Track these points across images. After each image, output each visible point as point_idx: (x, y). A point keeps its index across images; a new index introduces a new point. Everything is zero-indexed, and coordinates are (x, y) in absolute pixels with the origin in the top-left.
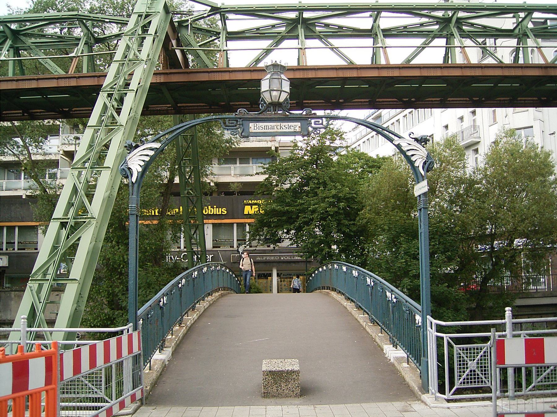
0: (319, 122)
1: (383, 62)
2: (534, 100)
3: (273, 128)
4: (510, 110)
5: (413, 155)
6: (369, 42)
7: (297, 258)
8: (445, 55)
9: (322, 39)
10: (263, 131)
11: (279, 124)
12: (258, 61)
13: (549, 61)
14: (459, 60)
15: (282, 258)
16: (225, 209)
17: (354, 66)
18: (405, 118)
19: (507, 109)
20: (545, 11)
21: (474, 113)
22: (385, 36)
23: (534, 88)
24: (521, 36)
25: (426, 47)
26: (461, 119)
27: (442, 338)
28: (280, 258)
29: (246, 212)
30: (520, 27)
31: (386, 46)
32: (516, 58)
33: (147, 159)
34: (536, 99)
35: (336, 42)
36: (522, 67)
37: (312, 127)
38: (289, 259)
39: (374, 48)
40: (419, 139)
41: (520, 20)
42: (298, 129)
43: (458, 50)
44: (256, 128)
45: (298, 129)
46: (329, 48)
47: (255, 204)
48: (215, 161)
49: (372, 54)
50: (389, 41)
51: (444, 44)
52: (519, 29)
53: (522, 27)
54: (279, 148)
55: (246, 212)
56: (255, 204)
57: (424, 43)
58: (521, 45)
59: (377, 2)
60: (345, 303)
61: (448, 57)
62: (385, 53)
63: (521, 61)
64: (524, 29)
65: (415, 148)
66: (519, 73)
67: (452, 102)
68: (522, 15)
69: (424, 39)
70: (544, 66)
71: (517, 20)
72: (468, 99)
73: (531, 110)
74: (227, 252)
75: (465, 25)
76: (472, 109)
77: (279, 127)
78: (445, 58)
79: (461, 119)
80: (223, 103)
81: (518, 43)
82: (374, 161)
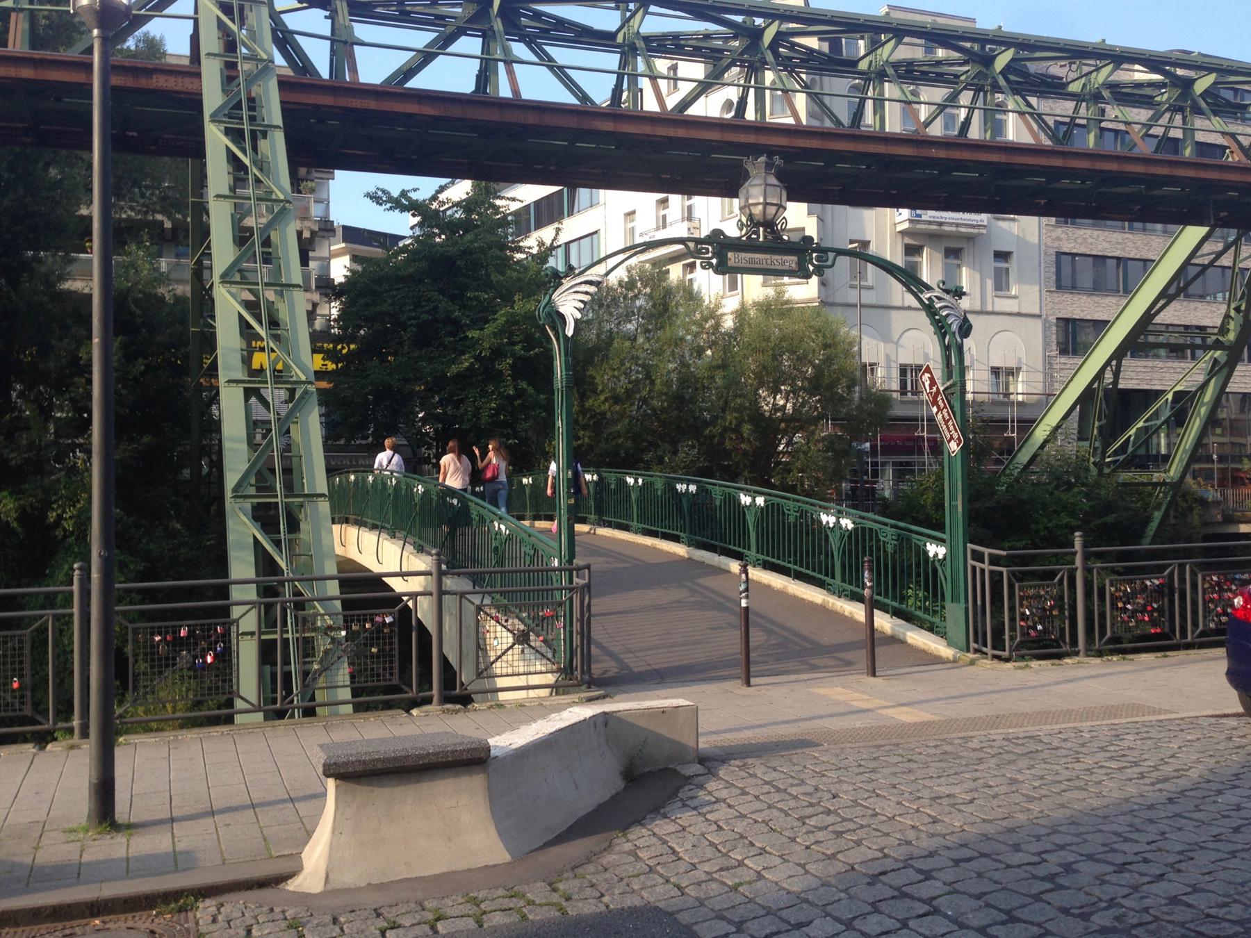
1: (505, 91)
3: (760, 262)
6: (611, 60)
8: (616, 86)
10: (748, 265)
11: (768, 256)
12: (409, 72)
19: (710, 198)
21: (664, 202)
25: (439, 54)
26: (631, 214)
27: (1001, 573)
32: (858, 114)
33: (586, 298)
35: (562, 55)
41: (628, 14)
43: (501, 65)
46: (547, 66)
51: (615, 67)
52: (871, 61)
59: (1104, 41)
62: (511, 73)
63: (750, 115)
71: (623, 15)
72: (650, 175)
75: (784, 47)
76: (661, 196)
77: (769, 262)
78: (614, 91)
79: (631, 214)
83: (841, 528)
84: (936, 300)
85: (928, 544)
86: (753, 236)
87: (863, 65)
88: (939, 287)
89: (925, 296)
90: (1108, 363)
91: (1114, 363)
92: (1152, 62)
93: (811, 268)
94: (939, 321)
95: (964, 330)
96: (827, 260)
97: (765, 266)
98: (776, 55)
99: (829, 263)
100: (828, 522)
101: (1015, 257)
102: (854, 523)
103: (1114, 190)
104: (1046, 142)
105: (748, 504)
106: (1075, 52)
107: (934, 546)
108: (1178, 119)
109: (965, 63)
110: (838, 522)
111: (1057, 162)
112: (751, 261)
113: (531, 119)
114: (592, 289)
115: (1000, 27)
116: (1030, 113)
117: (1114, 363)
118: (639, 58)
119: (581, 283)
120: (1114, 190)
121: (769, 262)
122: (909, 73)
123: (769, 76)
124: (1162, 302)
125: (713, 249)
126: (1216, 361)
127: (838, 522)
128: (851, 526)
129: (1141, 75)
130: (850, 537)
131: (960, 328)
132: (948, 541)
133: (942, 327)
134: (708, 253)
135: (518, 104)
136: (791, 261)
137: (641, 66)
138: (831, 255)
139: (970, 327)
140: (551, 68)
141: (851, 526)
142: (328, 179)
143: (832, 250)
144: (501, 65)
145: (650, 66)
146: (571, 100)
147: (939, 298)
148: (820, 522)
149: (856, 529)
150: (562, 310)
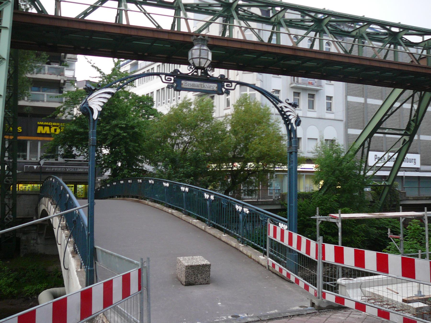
0: (229, 85)
1: (124, 22)
2: (277, 70)
4: (241, 72)
5: (290, 115)
6: (172, 12)
7: (80, 170)
9: (138, 4)
10: (191, 87)
11: (202, 83)
12: (86, 13)
13: (192, 32)
14: (184, 29)
15: (68, 170)
16: (21, 128)
17: (264, 44)
18: (159, 68)
20: (295, 9)
22: (187, 10)
23: (282, 62)
24: (276, 24)
28: (66, 170)
29: (39, 132)
30: (276, 17)
31: (128, 9)
33: (106, 101)
34: (235, 64)
36: (273, 46)
37: (225, 88)
38: (73, 170)
39: (118, 10)
40: (293, 104)
42: (215, 89)
44: (186, 85)
45: (215, 89)
47: (47, 126)
48: (30, 89)
49: (116, 14)
50: (190, 15)
52: (275, 19)
53: (277, 17)
54: (67, 81)
55: (39, 132)
56: (47, 126)
57: (212, 20)
58: (228, 24)
60: (191, 220)
61: (175, 25)
64: (279, 19)
65: (290, 110)
66: (225, 44)
67: (226, 65)
68: (278, 9)
69: (212, 17)
70: (243, 41)
73: (255, 74)
74: (21, 163)
77: (202, 86)
80: (50, 44)
81: (273, 29)
82: (140, 98)
83: (244, 212)
84: (284, 107)
85: (280, 223)
86: (195, 74)
87: (273, 20)
88: (286, 102)
89: (280, 105)
90: (366, 139)
91: (368, 139)
92: (383, 24)
93: (224, 90)
94: (286, 118)
95: (297, 122)
96: (231, 86)
97: (200, 88)
98: (238, 14)
99: (233, 88)
100: (239, 210)
101: (334, 98)
102: (249, 210)
103: (368, 73)
104: (342, 52)
105: (207, 198)
106: (355, 20)
107: (282, 224)
108: (392, 46)
109: (312, 22)
110: (243, 209)
111: (346, 60)
112: (193, 85)
113: (133, 33)
114: (109, 96)
115: (325, 9)
116: (337, 42)
117: (368, 139)
118: (181, 12)
119: (102, 93)
120: (368, 73)
121: (202, 86)
122: (291, 24)
123: (236, 22)
124: (344, 50)
125: (174, 78)
126: (405, 140)
127: (243, 209)
128: (248, 212)
129: (378, 28)
130: (247, 217)
131: (296, 122)
132: (288, 223)
133: (287, 121)
134: (171, 80)
135: (129, 27)
136: (214, 86)
137: (182, 15)
138: (234, 84)
139: (300, 121)
140: (145, 14)
141: (248, 212)
142: (75, 62)
143: (234, 82)
144: (123, 11)
145: (185, 15)
146: (153, 26)
147: (286, 107)
148: (236, 209)
149: (250, 213)
150: (92, 106)
